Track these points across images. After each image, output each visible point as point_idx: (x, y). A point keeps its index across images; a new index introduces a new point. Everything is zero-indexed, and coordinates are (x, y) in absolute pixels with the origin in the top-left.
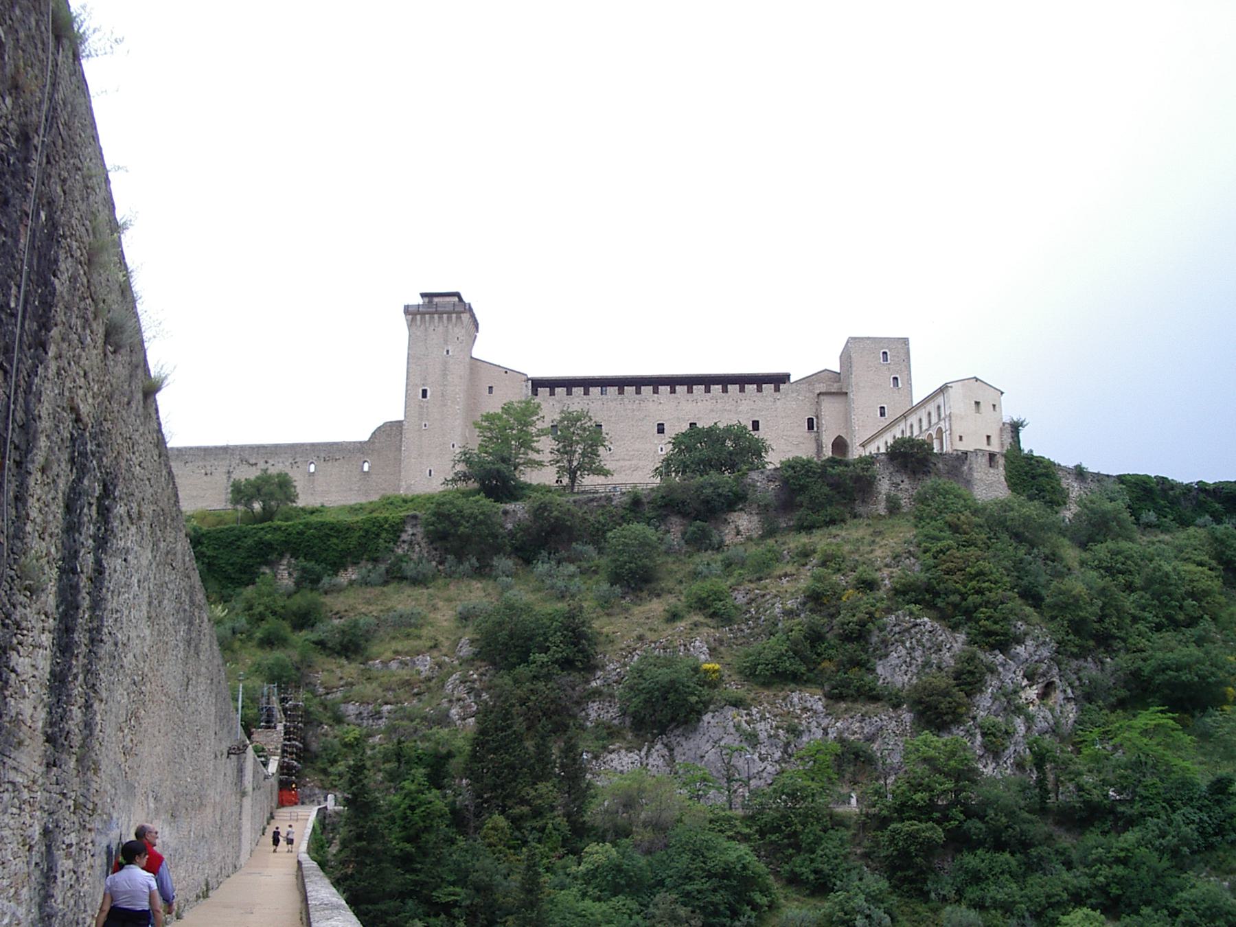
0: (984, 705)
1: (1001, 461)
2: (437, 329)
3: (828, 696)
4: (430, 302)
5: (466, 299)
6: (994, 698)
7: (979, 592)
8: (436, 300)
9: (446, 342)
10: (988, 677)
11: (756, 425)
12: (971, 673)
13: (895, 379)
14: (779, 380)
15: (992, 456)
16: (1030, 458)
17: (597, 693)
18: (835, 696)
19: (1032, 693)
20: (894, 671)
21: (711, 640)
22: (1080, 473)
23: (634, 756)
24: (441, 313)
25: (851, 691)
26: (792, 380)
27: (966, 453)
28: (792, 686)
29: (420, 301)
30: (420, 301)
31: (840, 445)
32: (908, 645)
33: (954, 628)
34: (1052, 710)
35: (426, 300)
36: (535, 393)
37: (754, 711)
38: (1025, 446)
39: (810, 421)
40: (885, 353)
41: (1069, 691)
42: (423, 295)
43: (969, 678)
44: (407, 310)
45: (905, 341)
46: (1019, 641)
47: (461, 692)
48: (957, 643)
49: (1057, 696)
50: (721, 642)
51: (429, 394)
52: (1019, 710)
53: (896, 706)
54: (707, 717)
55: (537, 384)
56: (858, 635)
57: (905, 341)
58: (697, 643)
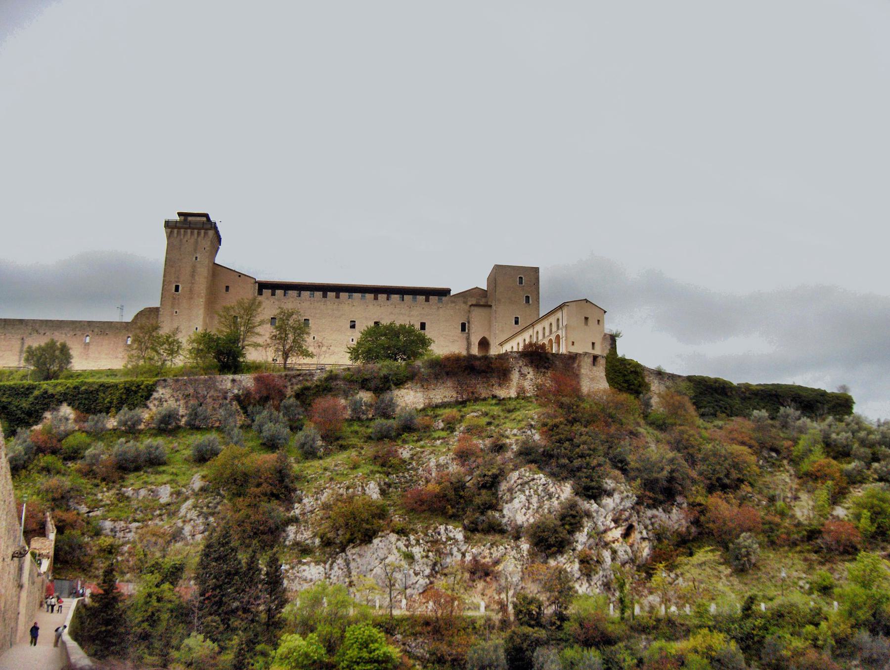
0: (581, 538)
1: (602, 362)
2: (189, 239)
3: (465, 528)
4: (185, 220)
5: (212, 219)
6: (590, 536)
7: (582, 456)
8: (190, 218)
9: (195, 250)
10: (585, 520)
11: (423, 326)
12: (574, 517)
13: (528, 297)
14: (443, 293)
15: (595, 358)
16: (623, 361)
17: (295, 520)
18: (472, 530)
19: (617, 533)
20: (518, 510)
21: (382, 483)
22: (660, 374)
23: (320, 568)
24: (193, 230)
25: (486, 526)
26: (452, 293)
27: (577, 354)
28: (440, 520)
29: (177, 218)
30: (177, 218)
31: (484, 344)
32: (527, 493)
33: (565, 479)
34: (631, 546)
35: (182, 218)
36: (260, 293)
37: (412, 537)
38: (620, 353)
39: (463, 325)
40: (521, 278)
41: (644, 532)
42: (180, 214)
43: (572, 519)
44: (168, 224)
45: (536, 270)
46: (610, 494)
47: (193, 514)
48: (566, 491)
49: (636, 536)
50: (389, 485)
51: (180, 288)
52: (606, 545)
53: (517, 538)
54: (376, 541)
55: (263, 286)
56: (492, 483)
57: (536, 270)
58: (537, 437)
